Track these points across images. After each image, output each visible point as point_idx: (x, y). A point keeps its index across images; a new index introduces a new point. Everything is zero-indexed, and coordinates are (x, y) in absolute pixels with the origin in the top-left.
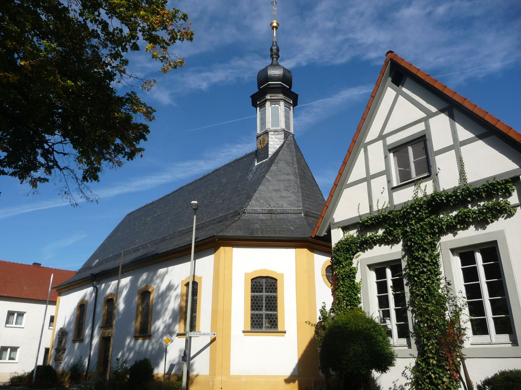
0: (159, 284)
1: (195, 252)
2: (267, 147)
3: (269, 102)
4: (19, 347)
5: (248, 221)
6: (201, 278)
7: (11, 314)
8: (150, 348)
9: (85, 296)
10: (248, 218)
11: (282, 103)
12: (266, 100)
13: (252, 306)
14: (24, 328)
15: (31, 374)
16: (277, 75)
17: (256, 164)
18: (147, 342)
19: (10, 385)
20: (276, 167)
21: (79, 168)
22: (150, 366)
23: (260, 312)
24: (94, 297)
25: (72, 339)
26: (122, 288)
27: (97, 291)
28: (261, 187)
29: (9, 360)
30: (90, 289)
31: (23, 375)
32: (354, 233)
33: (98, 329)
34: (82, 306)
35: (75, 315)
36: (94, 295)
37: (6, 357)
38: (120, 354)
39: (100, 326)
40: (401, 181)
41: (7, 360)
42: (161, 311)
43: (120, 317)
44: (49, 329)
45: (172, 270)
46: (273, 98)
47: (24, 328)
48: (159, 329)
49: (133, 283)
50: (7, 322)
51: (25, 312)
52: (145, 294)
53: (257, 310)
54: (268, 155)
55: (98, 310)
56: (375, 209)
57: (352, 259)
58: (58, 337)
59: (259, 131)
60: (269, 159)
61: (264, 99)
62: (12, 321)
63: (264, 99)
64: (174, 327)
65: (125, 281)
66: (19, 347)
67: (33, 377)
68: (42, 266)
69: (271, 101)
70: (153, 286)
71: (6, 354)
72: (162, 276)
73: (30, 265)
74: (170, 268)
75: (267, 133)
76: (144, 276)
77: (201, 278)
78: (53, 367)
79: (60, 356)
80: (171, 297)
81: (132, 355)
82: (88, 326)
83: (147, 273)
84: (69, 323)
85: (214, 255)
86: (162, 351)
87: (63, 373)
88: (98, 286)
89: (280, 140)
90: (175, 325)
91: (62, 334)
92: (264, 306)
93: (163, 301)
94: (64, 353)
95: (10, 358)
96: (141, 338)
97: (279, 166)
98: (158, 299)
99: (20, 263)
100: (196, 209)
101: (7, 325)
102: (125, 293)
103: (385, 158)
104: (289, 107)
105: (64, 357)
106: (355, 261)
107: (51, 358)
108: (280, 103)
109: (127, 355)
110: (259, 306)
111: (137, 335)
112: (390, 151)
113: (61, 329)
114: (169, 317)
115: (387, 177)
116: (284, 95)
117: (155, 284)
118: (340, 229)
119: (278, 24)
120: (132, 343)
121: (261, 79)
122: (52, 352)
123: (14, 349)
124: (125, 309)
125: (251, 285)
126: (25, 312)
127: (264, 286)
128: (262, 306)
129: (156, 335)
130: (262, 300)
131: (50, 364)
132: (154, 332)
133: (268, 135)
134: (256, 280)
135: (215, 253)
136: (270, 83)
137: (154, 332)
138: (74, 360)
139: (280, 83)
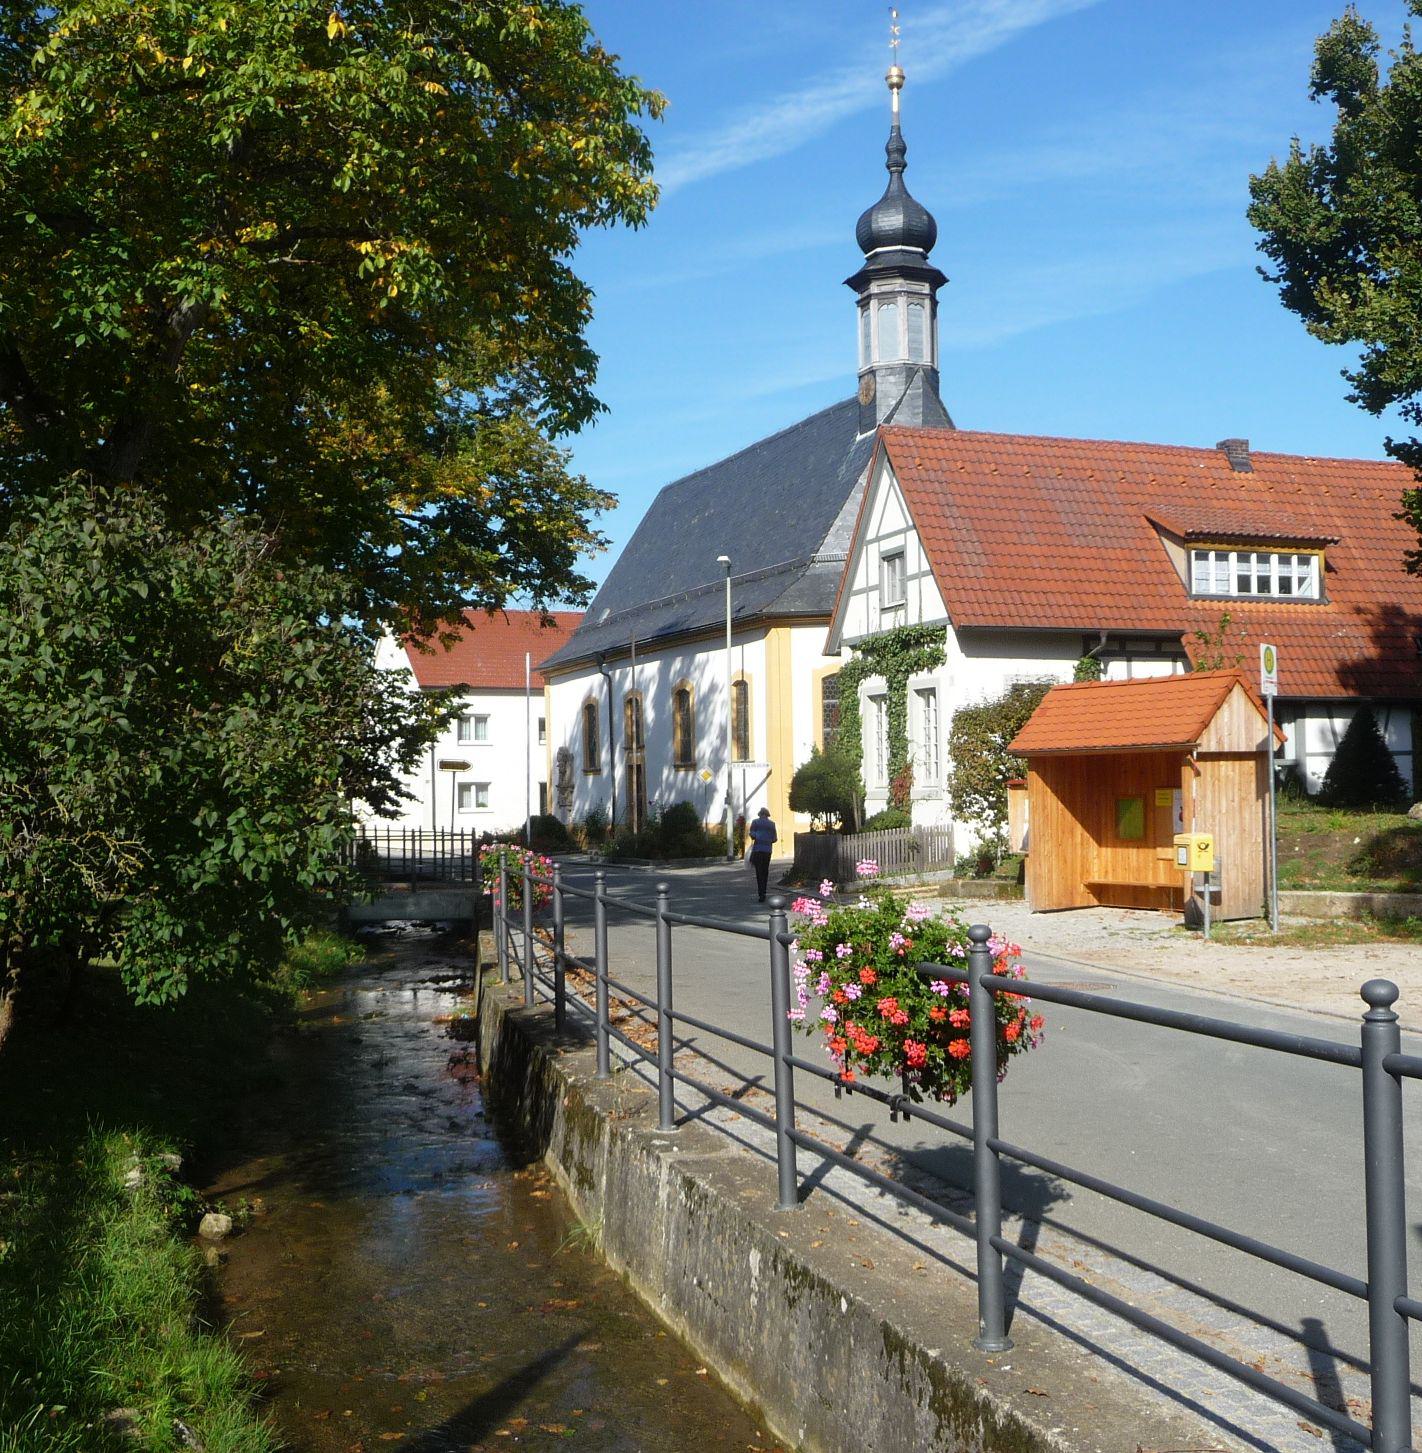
2: (872, 405)
5: (819, 577)
8: (696, 785)
9: (591, 690)
11: (902, 300)
12: (869, 297)
17: (859, 437)
18: (691, 774)
25: (582, 767)
27: (609, 680)
30: (598, 678)
34: (589, 709)
36: (605, 687)
46: (885, 289)
49: (664, 672)
52: (682, 695)
55: (616, 718)
74: (712, 654)
76: (677, 664)
78: (559, 817)
84: (573, 740)
86: (709, 791)
87: (575, 829)
91: (564, 758)
93: (706, 709)
95: (480, 805)
113: (561, 749)
122: (552, 791)
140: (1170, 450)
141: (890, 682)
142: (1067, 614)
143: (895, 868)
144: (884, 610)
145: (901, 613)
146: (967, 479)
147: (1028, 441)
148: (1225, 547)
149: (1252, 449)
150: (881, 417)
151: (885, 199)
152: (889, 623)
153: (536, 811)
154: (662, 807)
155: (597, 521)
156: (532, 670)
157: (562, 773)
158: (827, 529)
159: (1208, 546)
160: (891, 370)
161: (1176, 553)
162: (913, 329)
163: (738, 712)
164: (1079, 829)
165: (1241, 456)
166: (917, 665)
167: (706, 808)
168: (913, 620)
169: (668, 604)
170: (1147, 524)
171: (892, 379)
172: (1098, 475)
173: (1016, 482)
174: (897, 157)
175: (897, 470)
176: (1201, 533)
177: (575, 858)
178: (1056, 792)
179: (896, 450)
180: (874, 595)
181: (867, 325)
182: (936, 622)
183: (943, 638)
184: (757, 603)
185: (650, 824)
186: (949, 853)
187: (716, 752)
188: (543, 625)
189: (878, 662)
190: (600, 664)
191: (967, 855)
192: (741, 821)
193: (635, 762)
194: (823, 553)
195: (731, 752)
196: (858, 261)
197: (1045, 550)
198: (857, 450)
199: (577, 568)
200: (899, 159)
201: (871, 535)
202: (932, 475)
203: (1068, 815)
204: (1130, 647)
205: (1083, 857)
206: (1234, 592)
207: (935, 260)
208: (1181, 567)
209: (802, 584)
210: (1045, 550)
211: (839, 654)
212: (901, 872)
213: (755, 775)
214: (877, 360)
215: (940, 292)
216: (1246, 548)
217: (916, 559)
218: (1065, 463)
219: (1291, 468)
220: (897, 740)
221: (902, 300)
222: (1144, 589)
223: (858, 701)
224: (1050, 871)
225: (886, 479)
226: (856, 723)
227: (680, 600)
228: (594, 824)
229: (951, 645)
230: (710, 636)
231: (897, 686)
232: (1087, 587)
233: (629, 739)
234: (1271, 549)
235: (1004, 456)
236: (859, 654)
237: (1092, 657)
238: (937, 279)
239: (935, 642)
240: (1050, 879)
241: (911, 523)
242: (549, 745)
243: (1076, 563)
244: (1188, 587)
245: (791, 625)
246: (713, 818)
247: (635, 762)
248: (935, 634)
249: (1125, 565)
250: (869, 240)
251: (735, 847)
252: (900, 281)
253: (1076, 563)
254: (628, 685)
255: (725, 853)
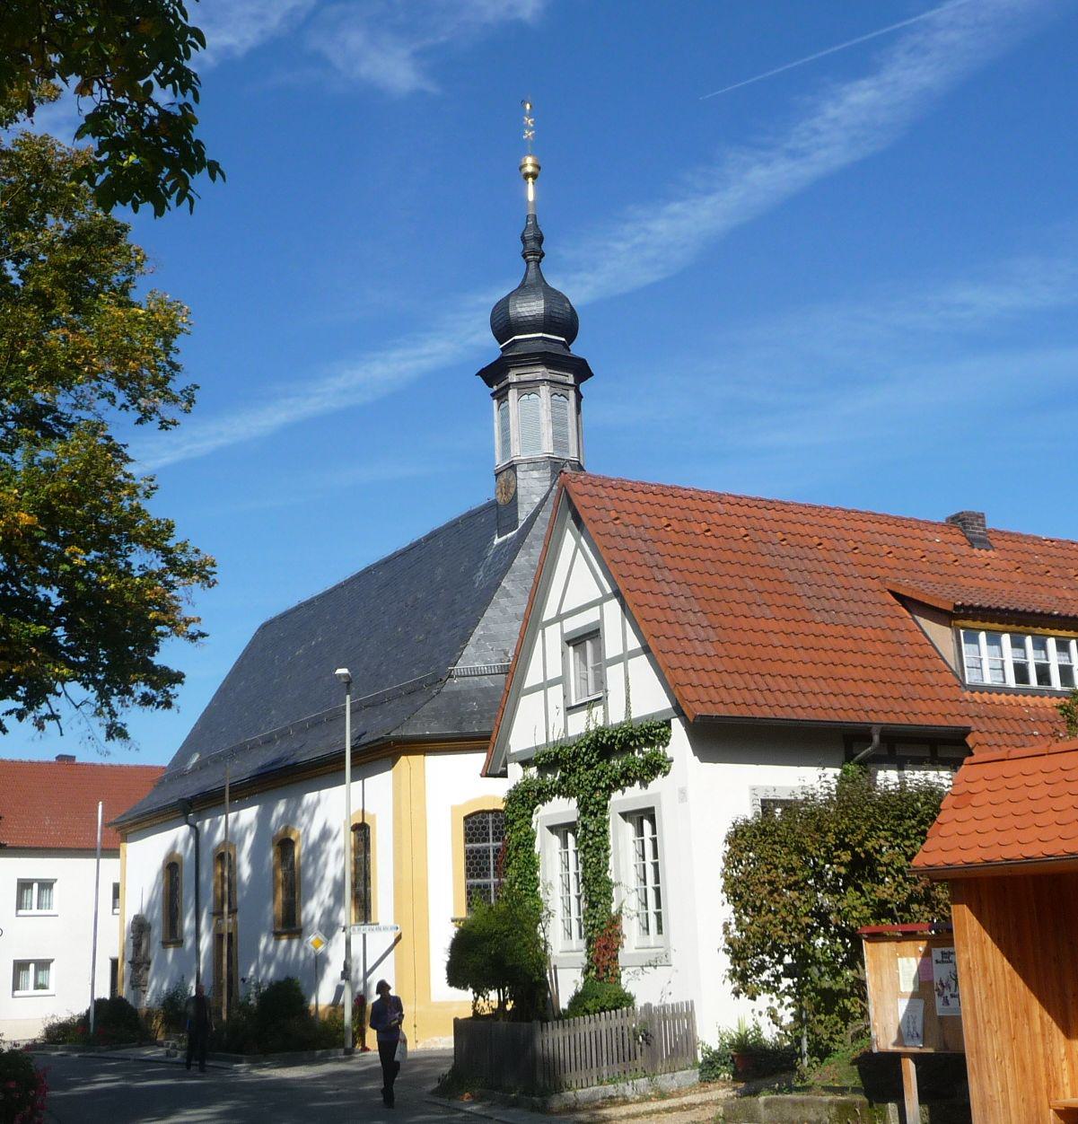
0: (307, 826)
1: (352, 767)
2: (513, 503)
3: (516, 390)
4: (52, 960)
5: (457, 694)
6: (374, 816)
7: (24, 885)
8: (302, 956)
9: (174, 846)
10: (457, 688)
11: (544, 390)
12: (508, 386)
13: (468, 870)
14: (57, 916)
15: (84, 1019)
16: (530, 319)
17: (497, 541)
18: (295, 943)
19: (46, 1042)
20: (527, 557)
21: (100, 725)
22: (297, 989)
23: (486, 880)
24: (192, 851)
25: (160, 939)
26: (243, 831)
27: (196, 832)
28: (489, 613)
29: (35, 989)
30: (183, 830)
31: (69, 1021)
32: (533, 771)
33: (208, 918)
34: (172, 867)
35: (159, 888)
36: (192, 842)
37: (27, 983)
38: (252, 969)
39: (212, 911)
40: (579, 696)
41: (31, 991)
42: (314, 881)
43: (245, 893)
44: (113, 914)
45: (327, 798)
46: (524, 378)
47: (57, 916)
48: (313, 917)
49: (263, 819)
50: (20, 906)
51: (56, 880)
52: (285, 845)
53: (478, 876)
54: (516, 521)
55: (203, 877)
56: (551, 740)
57: (530, 816)
58: (132, 935)
59: (500, 462)
60: (518, 533)
61: (503, 384)
62: (29, 902)
63: (503, 384)
64: (338, 915)
65: (248, 815)
66: (52, 960)
67: (89, 1024)
68: (77, 761)
69: (519, 386)
70: (297, 829)
71: (28, 976)
72: (312, 808)
73: (50, 763)
74: (324, 792)
75: (512, 467)
76: (281, 808)
77: (374, 816)
78: (131, 1001)
79: (140, 977)
80: (328, 854)
81: (272, 970)
82: (188, 910)
83: (285, 800)
84: (151, 906)
85: (391, 771)
86: (320, 963)
87: (150, 1014)
88: (198, 824)
89: (541, 484)
90: (339, 911)
91: (140, 928)
92: (492, 868)
93: (316, 860)
94: (148, 969)
95: (38, 986)
96: (285, 937)
97: (533, 555)
98: (308, 858)
99: (27, 760)
100: (348, 682)
101: (20, 912)
102: (249, 841)
103: (563, 653)
104: (564, 392)
105: (149, 978)
106: (534, 818)
107: (123, 982)
108: (539, 390)
109: (263, 972)
110: (482, 869)
111: (279, 929)
112: (568, 643)
113: (136, 917)
114: (328, 894)
115: (564, 688)
116: (548, 368)
117: (301, 826)
118: (517, 764)
119: (538, 167)
120: (271, 947)
121: (499, 328)
122: (124, 968)
123: (43, 965)
124: (254, 876)
125: (465, 829)
126: (56, 880)
127: (491, 828)
128: (488, 869)
129: (309, 929)
130: (488, 857)
131: (124, 996)
132: (307, 924)
133: (515, 472)
134: (474, 818)
135: (393, 767)
136: (517, 337)
137: (307, 924)
138: (170, 984)
139: (540, 335)
140: (898, 521)
141: (584, 808)
142: (826, 705)
143: (617, 1068)
144: (570, 710)
145: (598, 710)
146: (675, 538)
147: (739, 501)
148: (996, 626)
149: (989, 526)
150: (523, 516)
151: (522, 286)
152: (579, 725)
153: (104, 992)
154: (258, 986)
155: (191, 599)
156: (105, 825)
157: (137, 946)
158: (465, 639)
159: (978, 624)
160: (533, 464)
161: (940, 635)
162: (558, 422)
163: (356, 863)
164: (1036, 1008)
165: (977, 532)
166: (625, 779)
167: (314, 987)
168: (617, 716)
169: (269, 741)
170: (893, 600)
171: (535, 474)
172: (826, 543)
173: (734, 545)
174: (534, 247)
175: (589, 526)
176: (971, 606)
177: (149, 1052)
178: (997, 941)
179: (585, 500)
180: (556, 692)
181: (505, 418)
182: (653, 716)
183: (664, 739)
184: (382, 726)
185: (244, 1007)
186: (687, 1042)
187: (329, 913)
188: (109, 736)
189: (563, 780)
190: (186, 814)
191: (715, 1047)
192: (360, 1001)
193: (226, 929)
194: (461, 666)
195: (346, 914)
196: (491, 349)
197: (783, 625)
198: (495, 555)
199: (158, 660)
200: (536, 247)
201: (549, 612)
202: (634, 531)
203: (1020, 983)
204: (901, 751)
205: (1046, 1058)
206: (1011, 682)
207: (577, 349)
208: (947, 650)
209: (438, 702)
210: (783, 625)
211: (504, 775)
212: (623, 1076)
213: (378, 941)
214: (517, 452)
215: (583, 387)
216: (1021, 628)
217: (618, 634)
218: (788, 527)
219: (1032, 548)
220: (595, 886)
221: (544, 390)
222: (910, 677)
223: (534, 833)
224: (1004, 1090)
225: (569, 540)
226: (531, 864)
227: (283, 734)
228: (172, 1004)
229: (679, 743)
230: (326, 771)
231: (593, 809)
232: (840, 671)
233: (219, 902)
234: (1048, 631)
235: (716, 515)
236: (533, 771)
237: (860, 763)
238: (582, 371)
239: (650, 743)
240: (1006, 1104)
241: (609, 590)
242: (122, 915)
243: (824, 643)
244: (959, 675)
245: (425, 752)
246: (323, 997)
247: (226, 929)
248: (654, 733)
249: (880, 647)
250: (504, 326)
251: (354, 1035)
252: (542, 369)
253: (824, 643)
254: (219, 836)
255: (342, 1044)
